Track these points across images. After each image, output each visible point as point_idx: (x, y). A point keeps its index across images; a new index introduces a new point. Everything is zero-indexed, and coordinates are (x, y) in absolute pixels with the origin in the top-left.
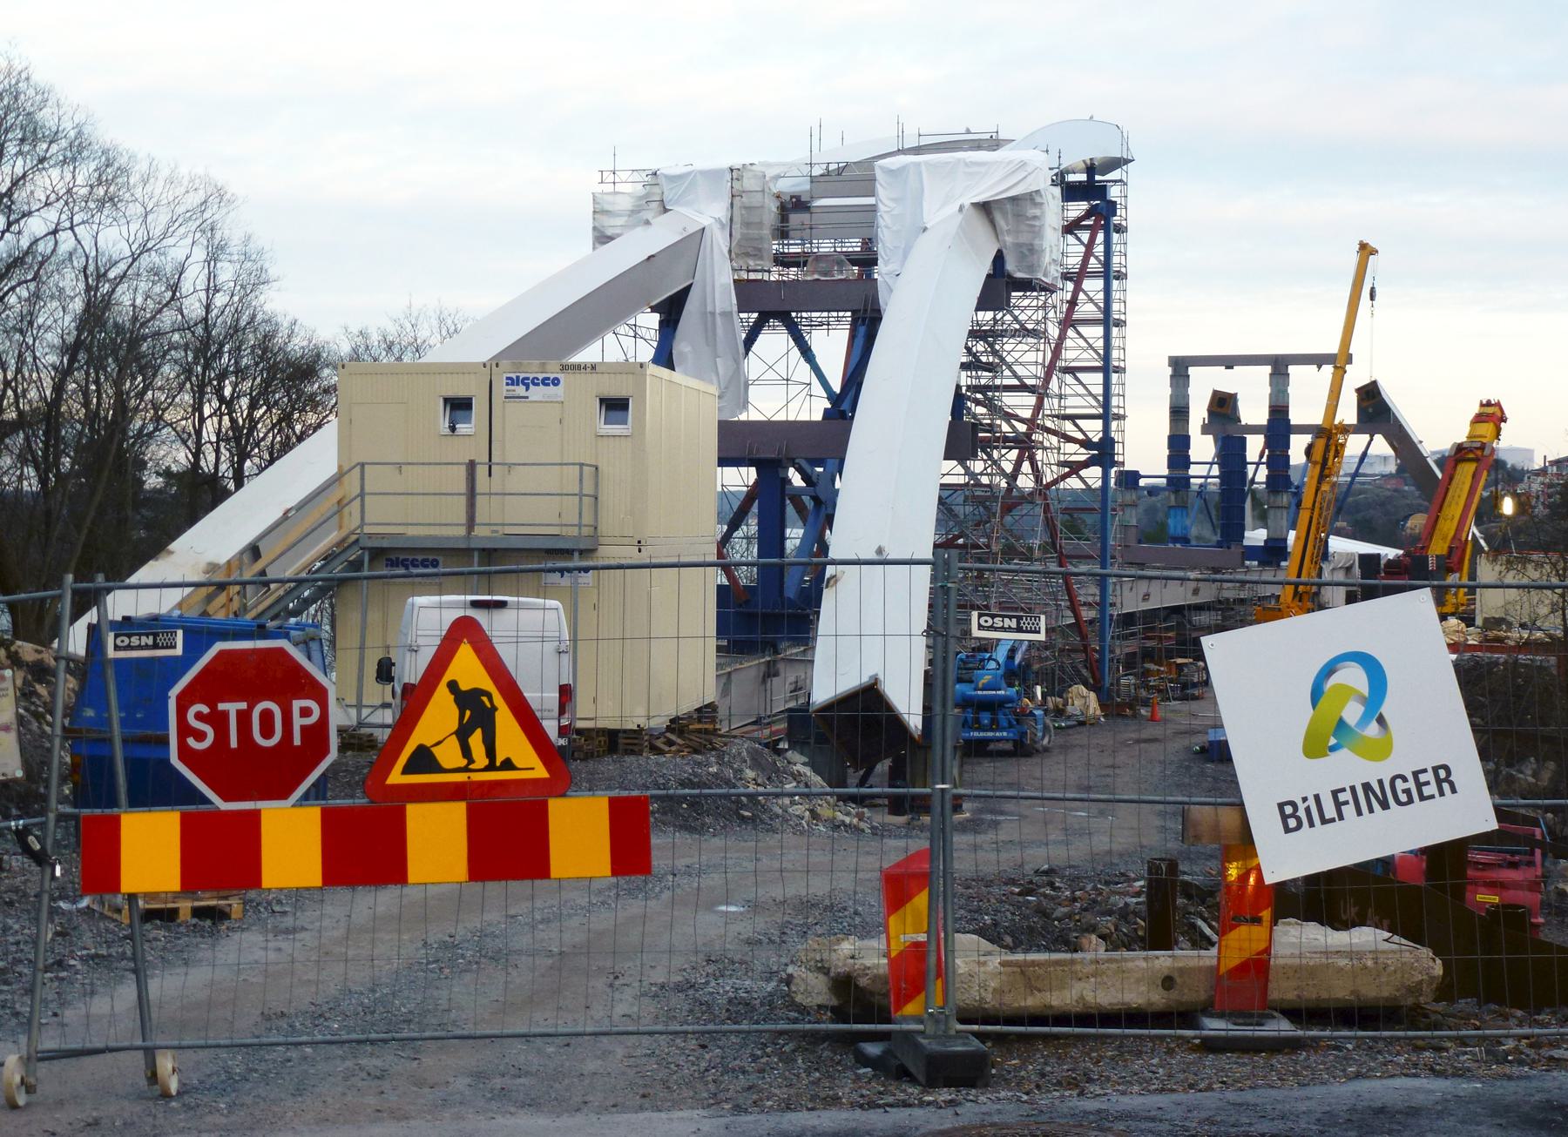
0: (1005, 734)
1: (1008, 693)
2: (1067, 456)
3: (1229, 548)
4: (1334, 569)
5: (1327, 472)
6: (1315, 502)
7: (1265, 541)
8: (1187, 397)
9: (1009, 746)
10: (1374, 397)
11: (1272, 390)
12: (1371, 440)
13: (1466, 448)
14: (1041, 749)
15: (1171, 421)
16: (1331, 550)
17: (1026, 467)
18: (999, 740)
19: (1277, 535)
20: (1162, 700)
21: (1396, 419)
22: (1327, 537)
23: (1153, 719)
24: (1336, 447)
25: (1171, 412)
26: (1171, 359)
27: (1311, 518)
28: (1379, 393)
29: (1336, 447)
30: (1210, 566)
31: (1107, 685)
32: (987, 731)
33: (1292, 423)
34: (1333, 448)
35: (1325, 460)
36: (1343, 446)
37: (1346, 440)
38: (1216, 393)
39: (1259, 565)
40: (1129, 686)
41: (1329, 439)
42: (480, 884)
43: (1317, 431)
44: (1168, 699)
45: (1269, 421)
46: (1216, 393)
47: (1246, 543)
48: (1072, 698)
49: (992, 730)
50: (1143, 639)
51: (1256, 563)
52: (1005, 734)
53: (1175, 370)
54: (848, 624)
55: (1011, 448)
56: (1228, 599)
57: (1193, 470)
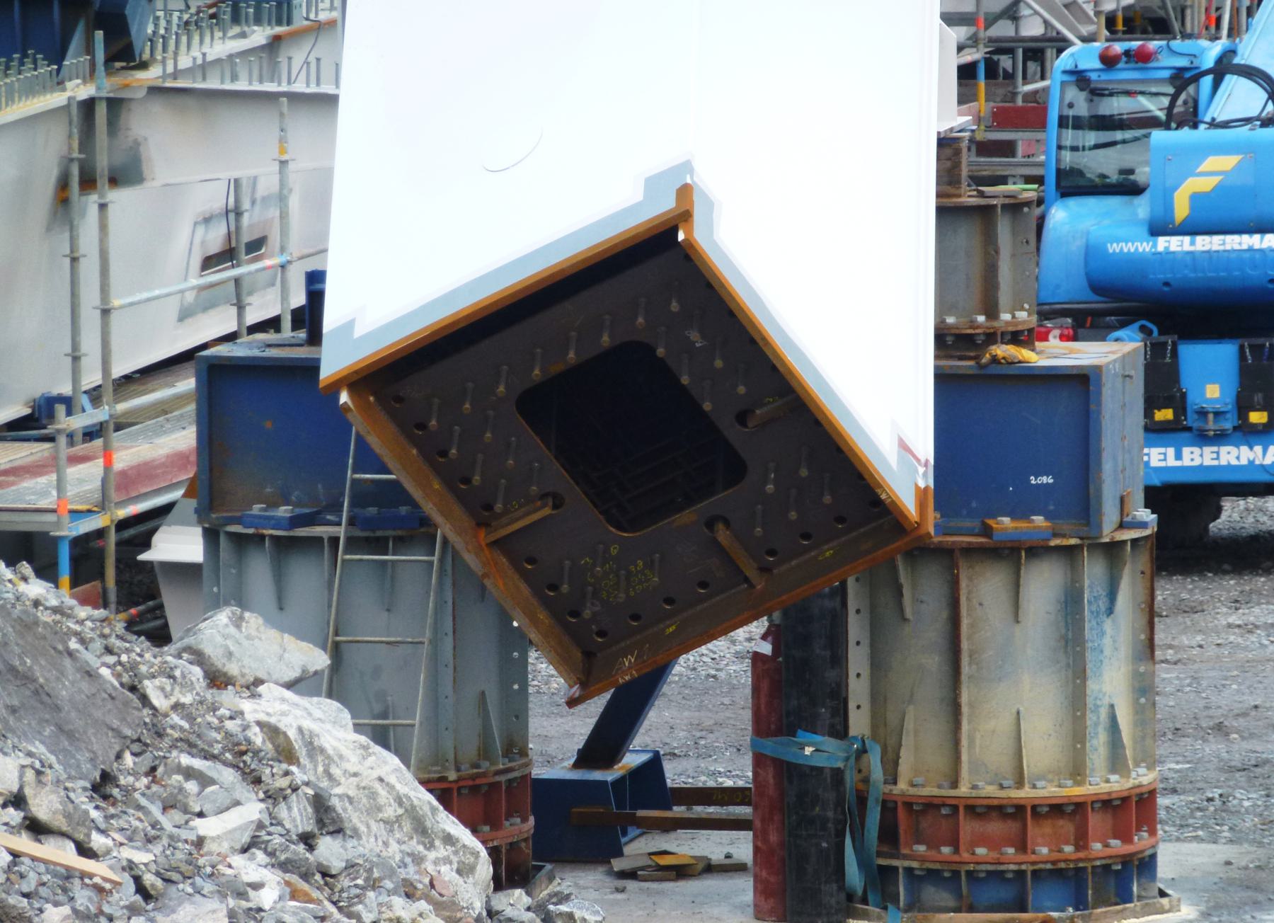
32: (1220, 438)
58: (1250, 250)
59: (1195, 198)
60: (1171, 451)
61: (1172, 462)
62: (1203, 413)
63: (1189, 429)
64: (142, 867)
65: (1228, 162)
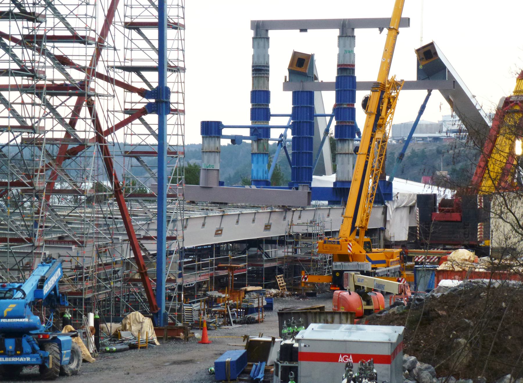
0: (28, 359)
1: (31, 321)
2: (133, 104)
3: (297, 189)
4: (397, 208)
5: (380, 121)
6: (369, 148)
7: (335, 184)
8: (266, 56)
9: (35, 370)
10: (431, 57)
11: (340, 50)
12: (429, 94)
13: (512, 102)
14: (69, 372)
15: (253, 77)
16: (395, 191)
17: (84, 112)
18: (26, 365)
19: (345, 178)
20: (224, 324)
21: (451, 76)
22: (391, 179)
23: (203, 341)
24: (389, 100)
25: (253, 71)
26: (253, 22)
27: (367, 162)
28: (436, 53)
29: (389, 100)
30: (281, 205)
31: (164, 310)
32: (12, 356)
33: (358, 80)
34: (386, 101)
35: (379, 111)
36: (395, 98)
37: (398, 93)
38: (295, 54)
39: (329, 204)
40: (191, 311)
41: (383, 92)
42: (214, 364)
43: (375, 87)
44: (229, 323)
45: (338, 78)
46: (295, 54)
47: (314, 184)
48: (130, 324)
49: (17, 355)
50: (216, 269)
51: (326, 202)
52: (28, 359)
53: (257, 33)
54: (404, 230)
55: (71, 95)
56: (298, 234)
57: (273, 122)
58: (18, 322)
59: (8, 312)
60: (3, 358)
61: (3, 360)
62: (8, 351)
63: (6, 354)
64: (494, 160)
65: (13, 306)
